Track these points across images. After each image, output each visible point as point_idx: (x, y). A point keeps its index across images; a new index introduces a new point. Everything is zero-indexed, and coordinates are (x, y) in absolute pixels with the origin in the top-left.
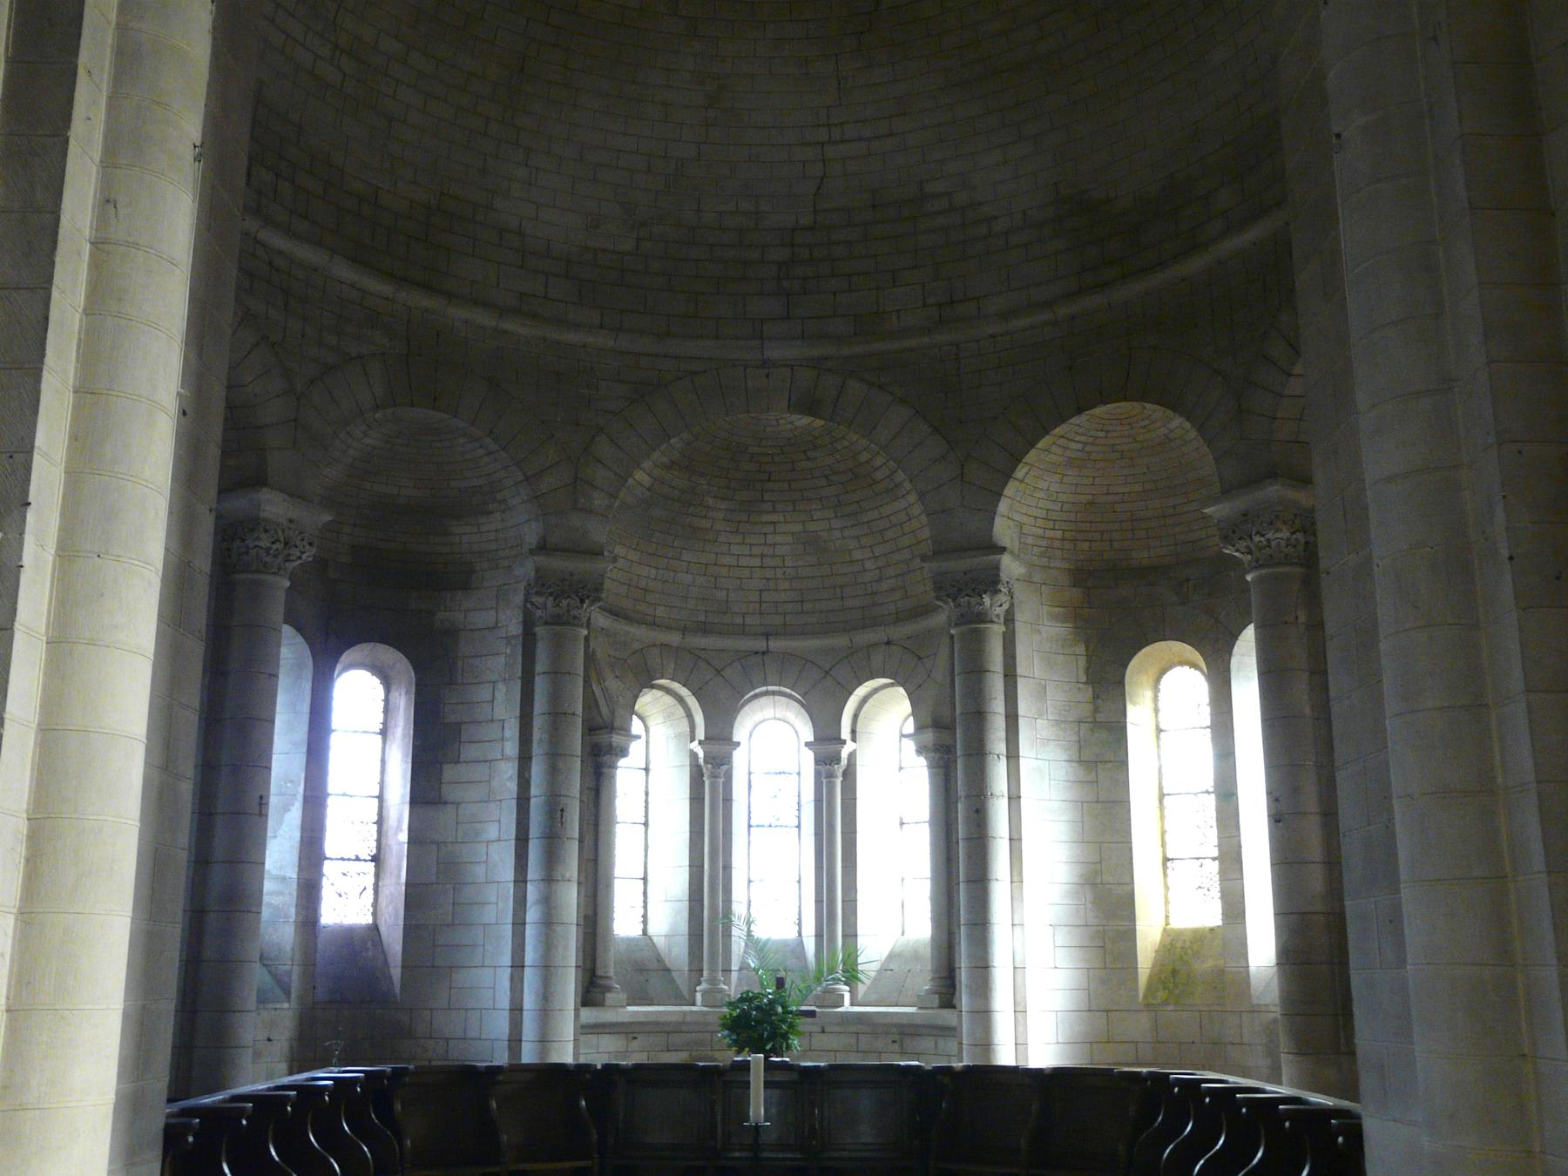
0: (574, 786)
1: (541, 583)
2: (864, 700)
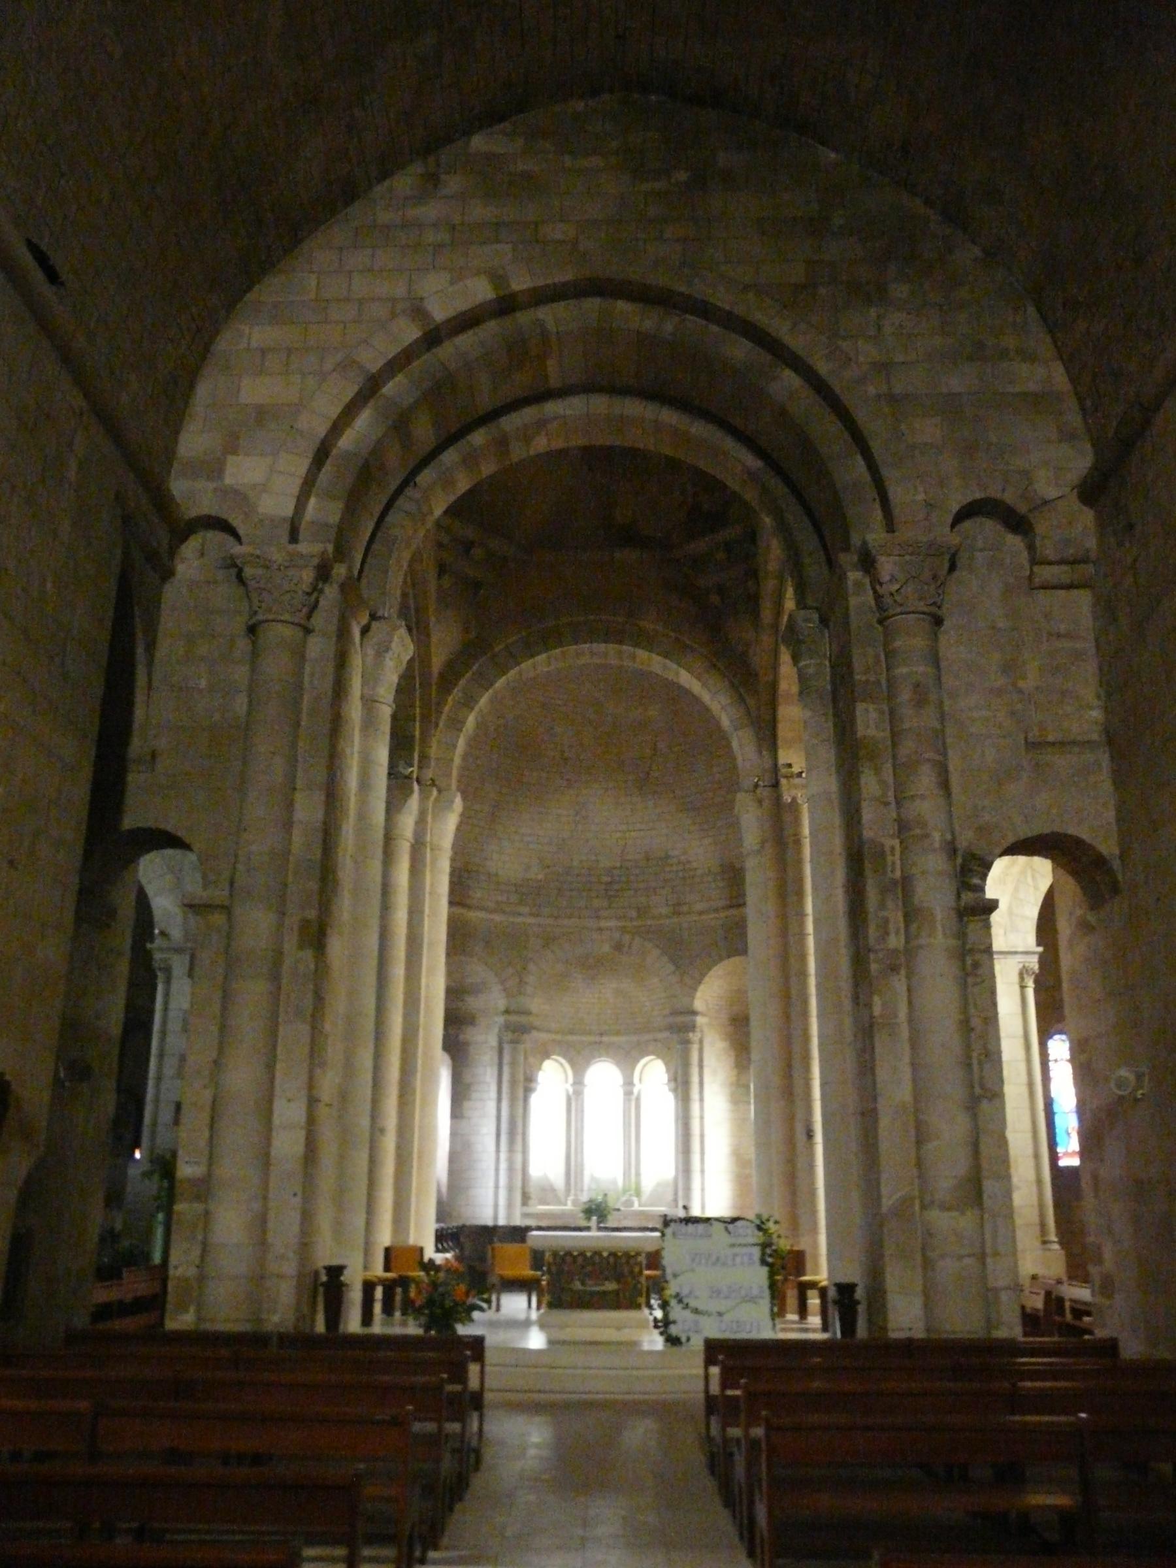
0: (520, 1111)
1: (507, 1027)
2: (645, 1066)
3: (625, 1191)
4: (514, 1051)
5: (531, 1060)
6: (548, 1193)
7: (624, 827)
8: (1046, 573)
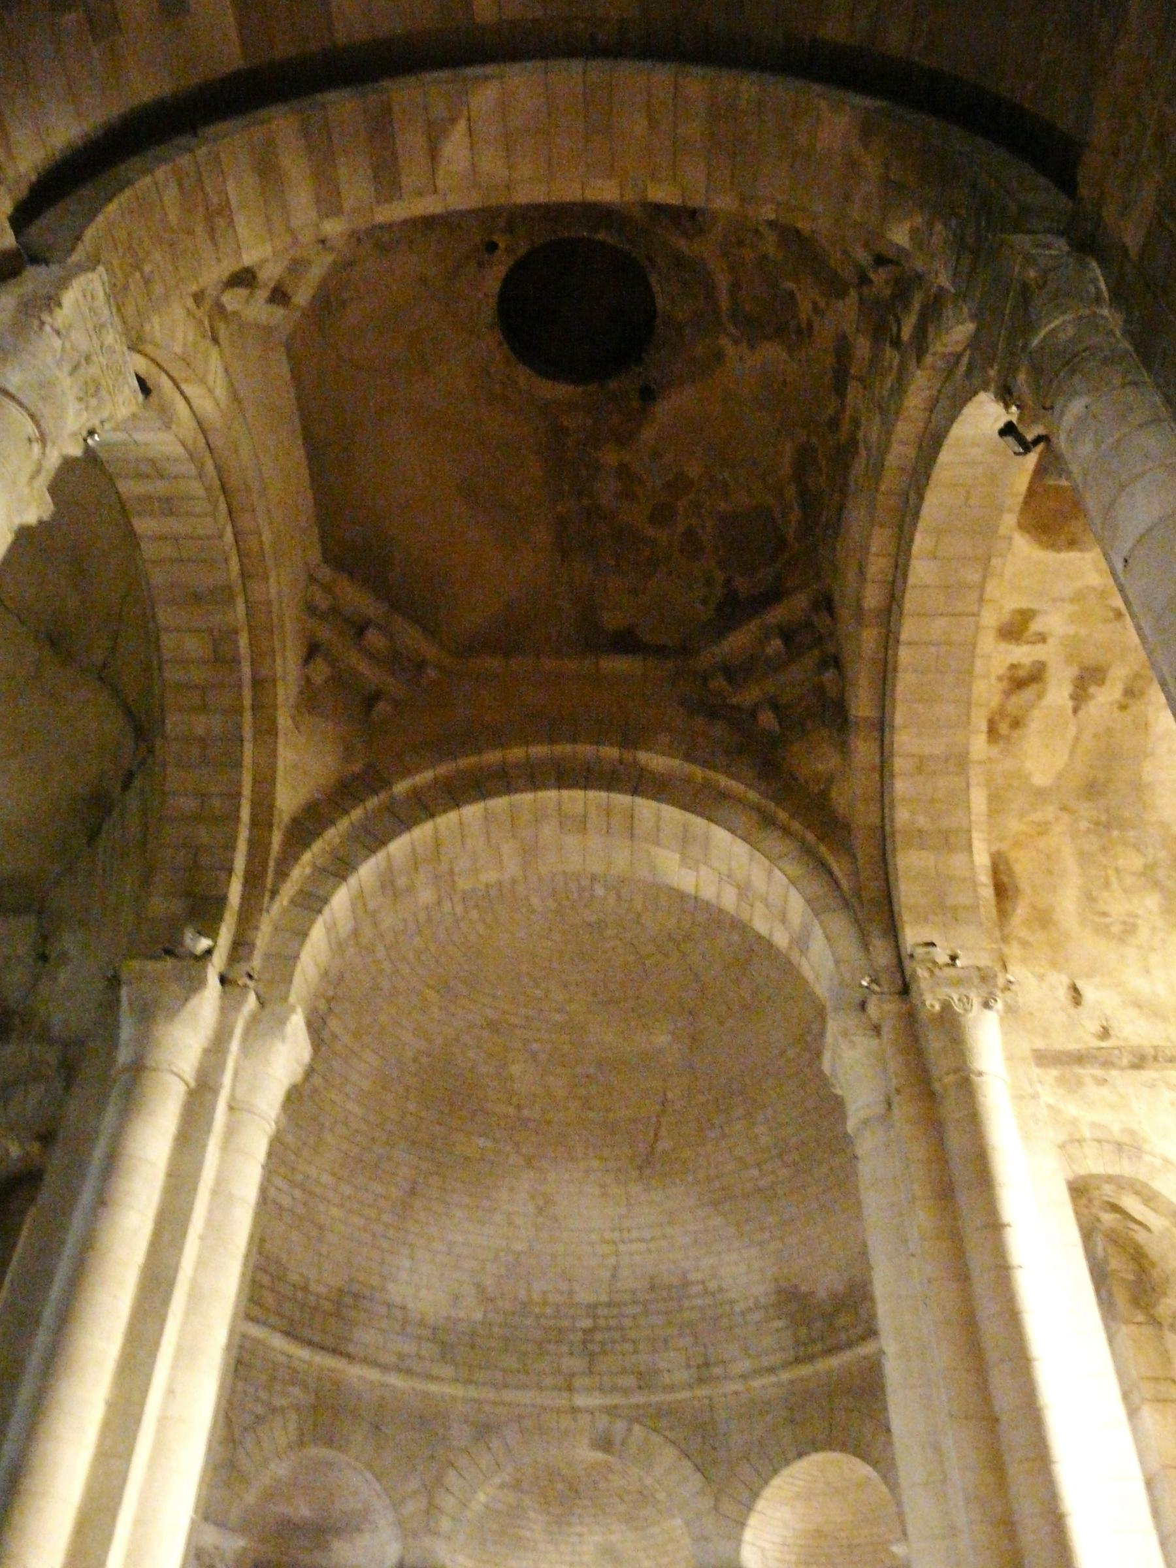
7: (616, 1235)
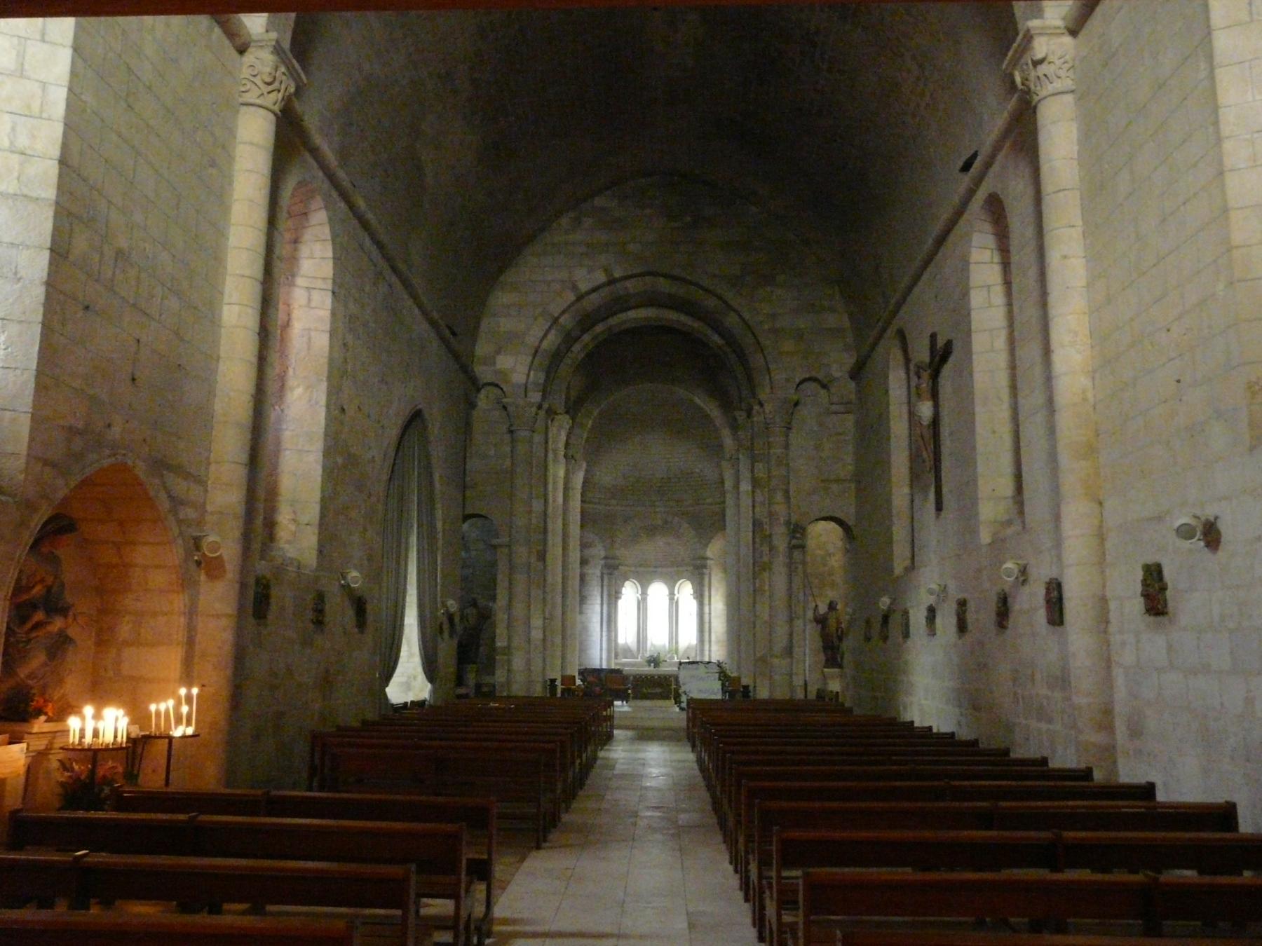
3: (669, 652)
4: (609, 579)
5: (618, 581)
6: (627, 651)
8: (834, 408)
